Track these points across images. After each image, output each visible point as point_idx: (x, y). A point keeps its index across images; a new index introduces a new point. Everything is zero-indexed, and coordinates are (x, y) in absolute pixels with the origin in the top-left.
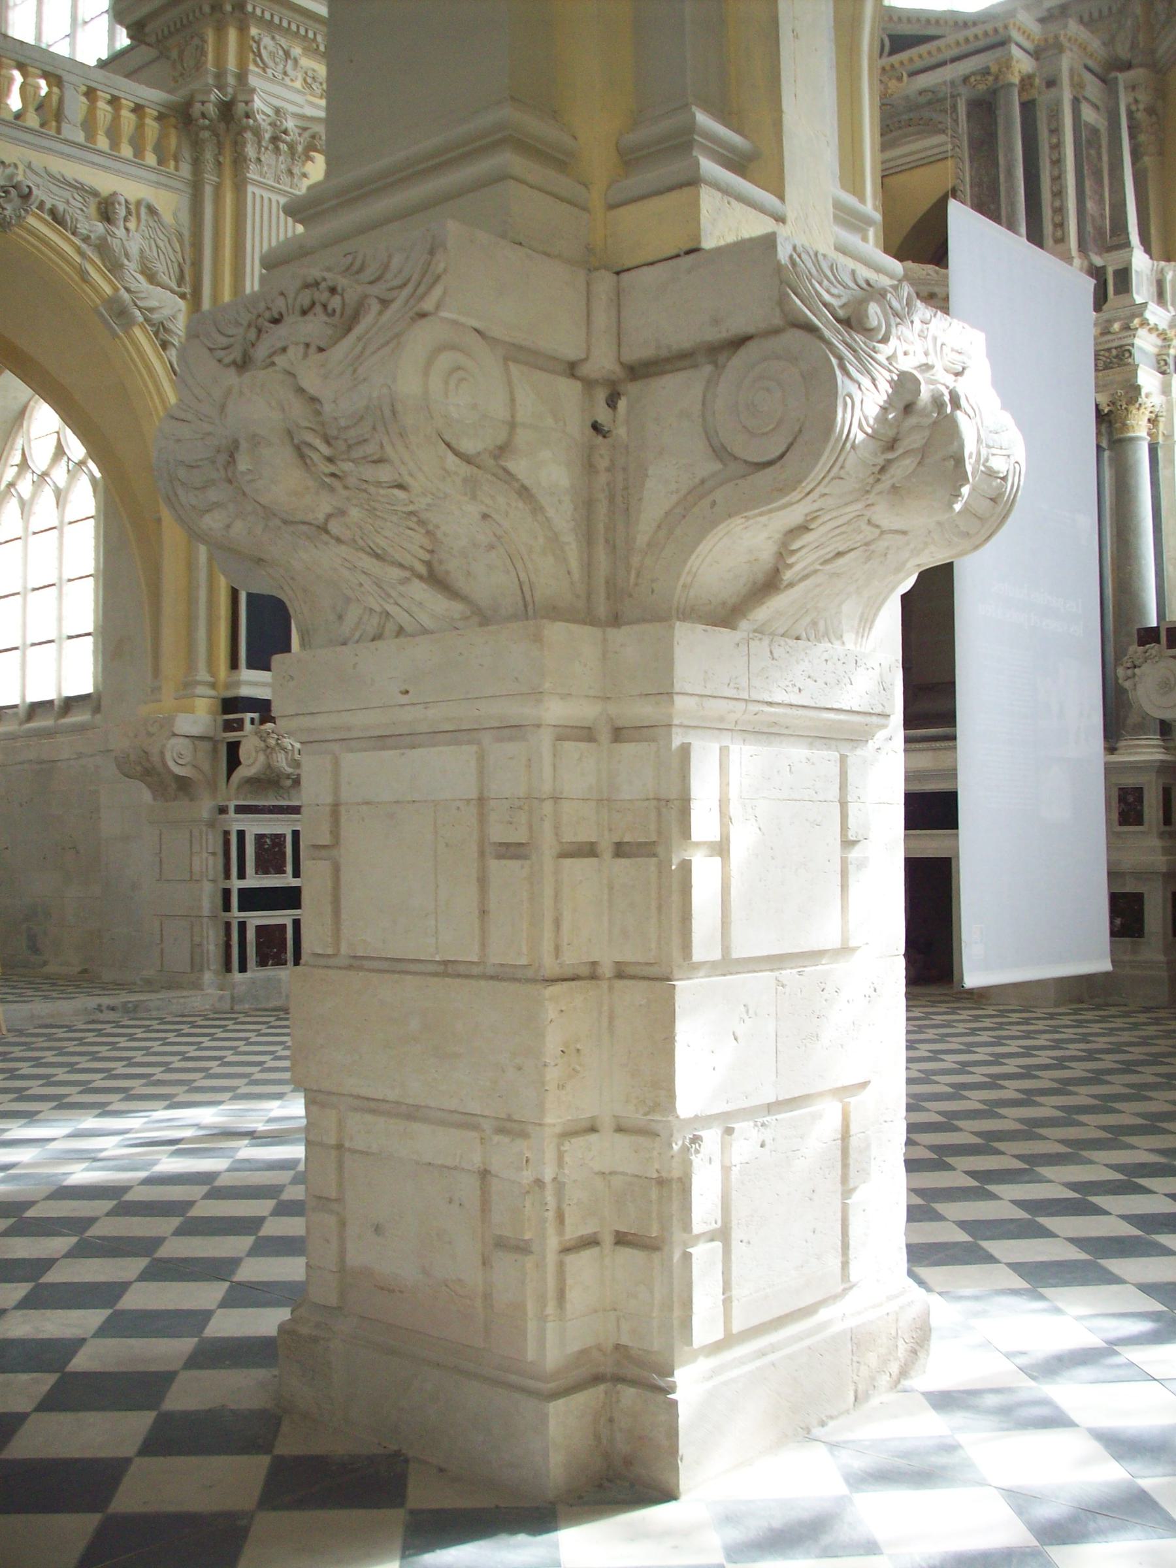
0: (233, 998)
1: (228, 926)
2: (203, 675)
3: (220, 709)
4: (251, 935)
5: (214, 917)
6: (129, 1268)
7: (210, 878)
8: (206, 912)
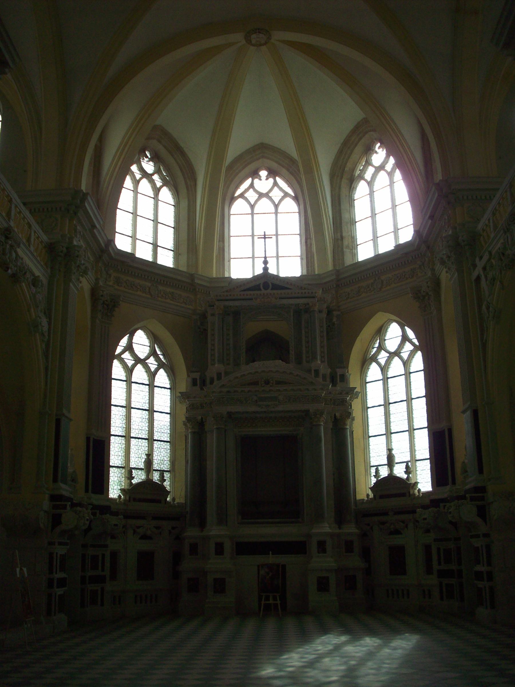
4: (100, 568)
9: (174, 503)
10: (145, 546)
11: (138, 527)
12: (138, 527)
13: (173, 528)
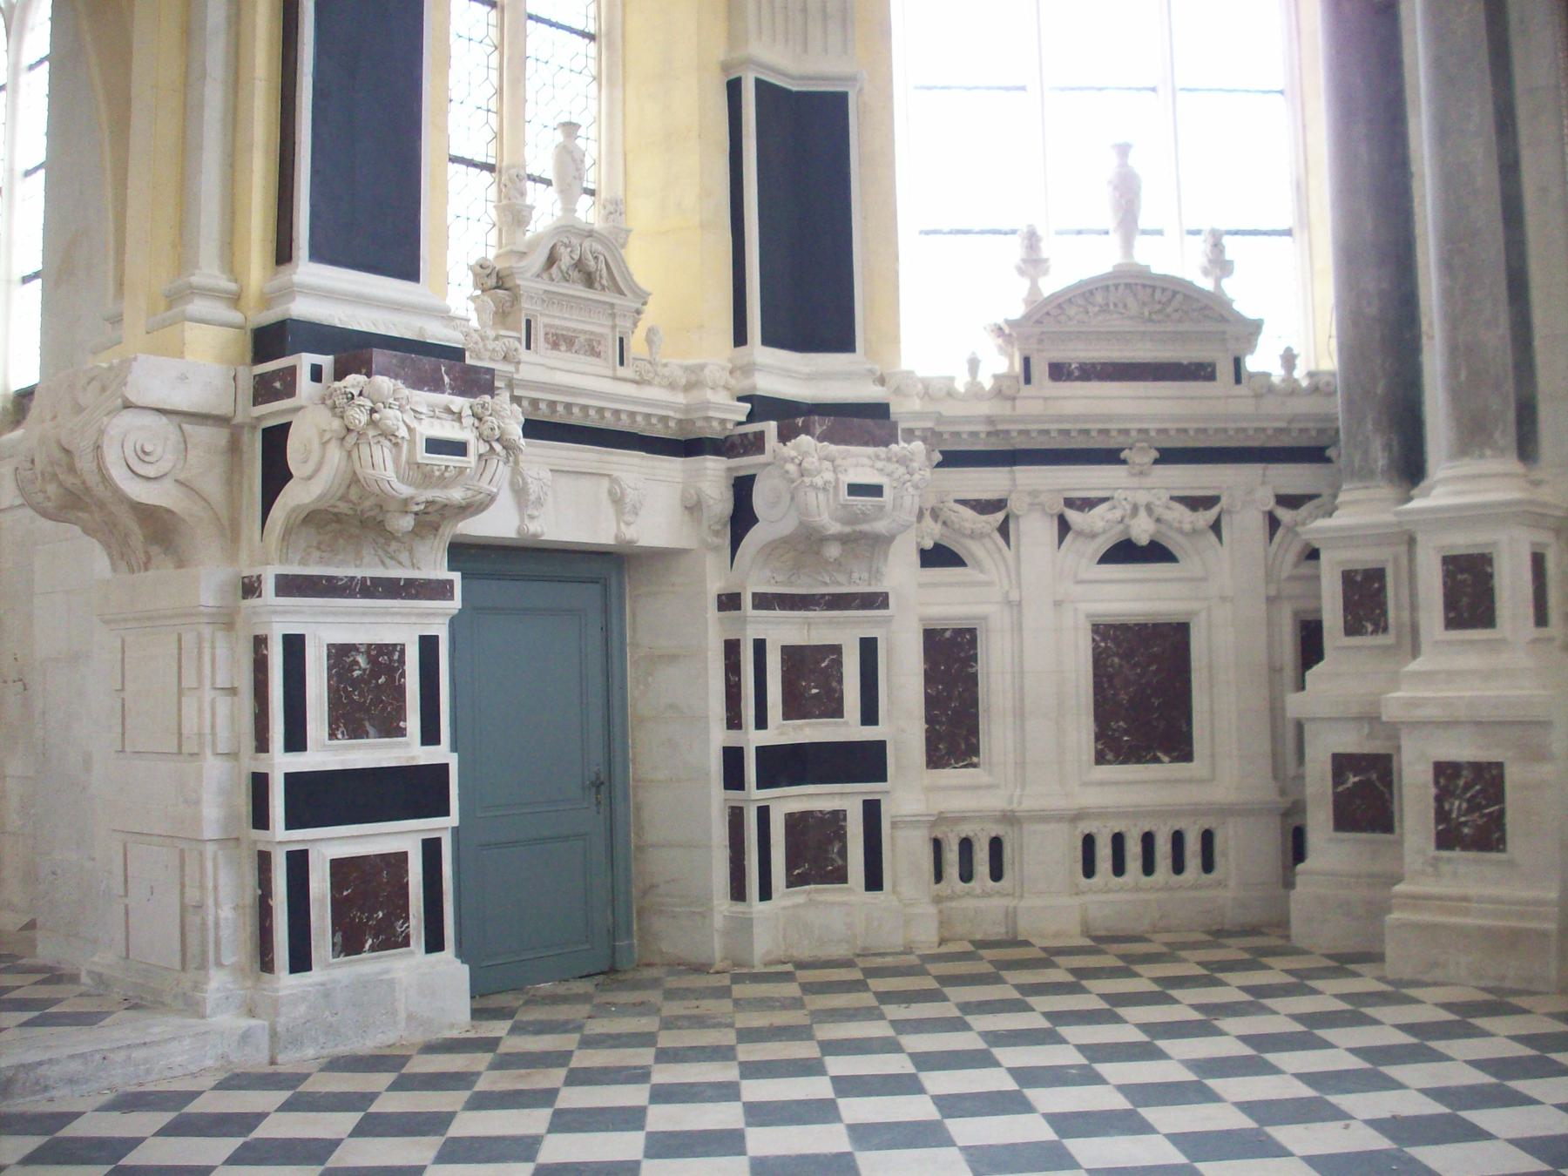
0: (274, 1035)
1: (264, 860)
2: (209, 272)
3: (249, 357)
4: (320, 884)
5: (230, 841)
6: (340, 1123)
7: (222, 748)
8: (210, 831)
9: (1289, 377)
10: (1135, 595)
11: (1086, 504)
12: (1086, 504)
13: (1290, 501)
